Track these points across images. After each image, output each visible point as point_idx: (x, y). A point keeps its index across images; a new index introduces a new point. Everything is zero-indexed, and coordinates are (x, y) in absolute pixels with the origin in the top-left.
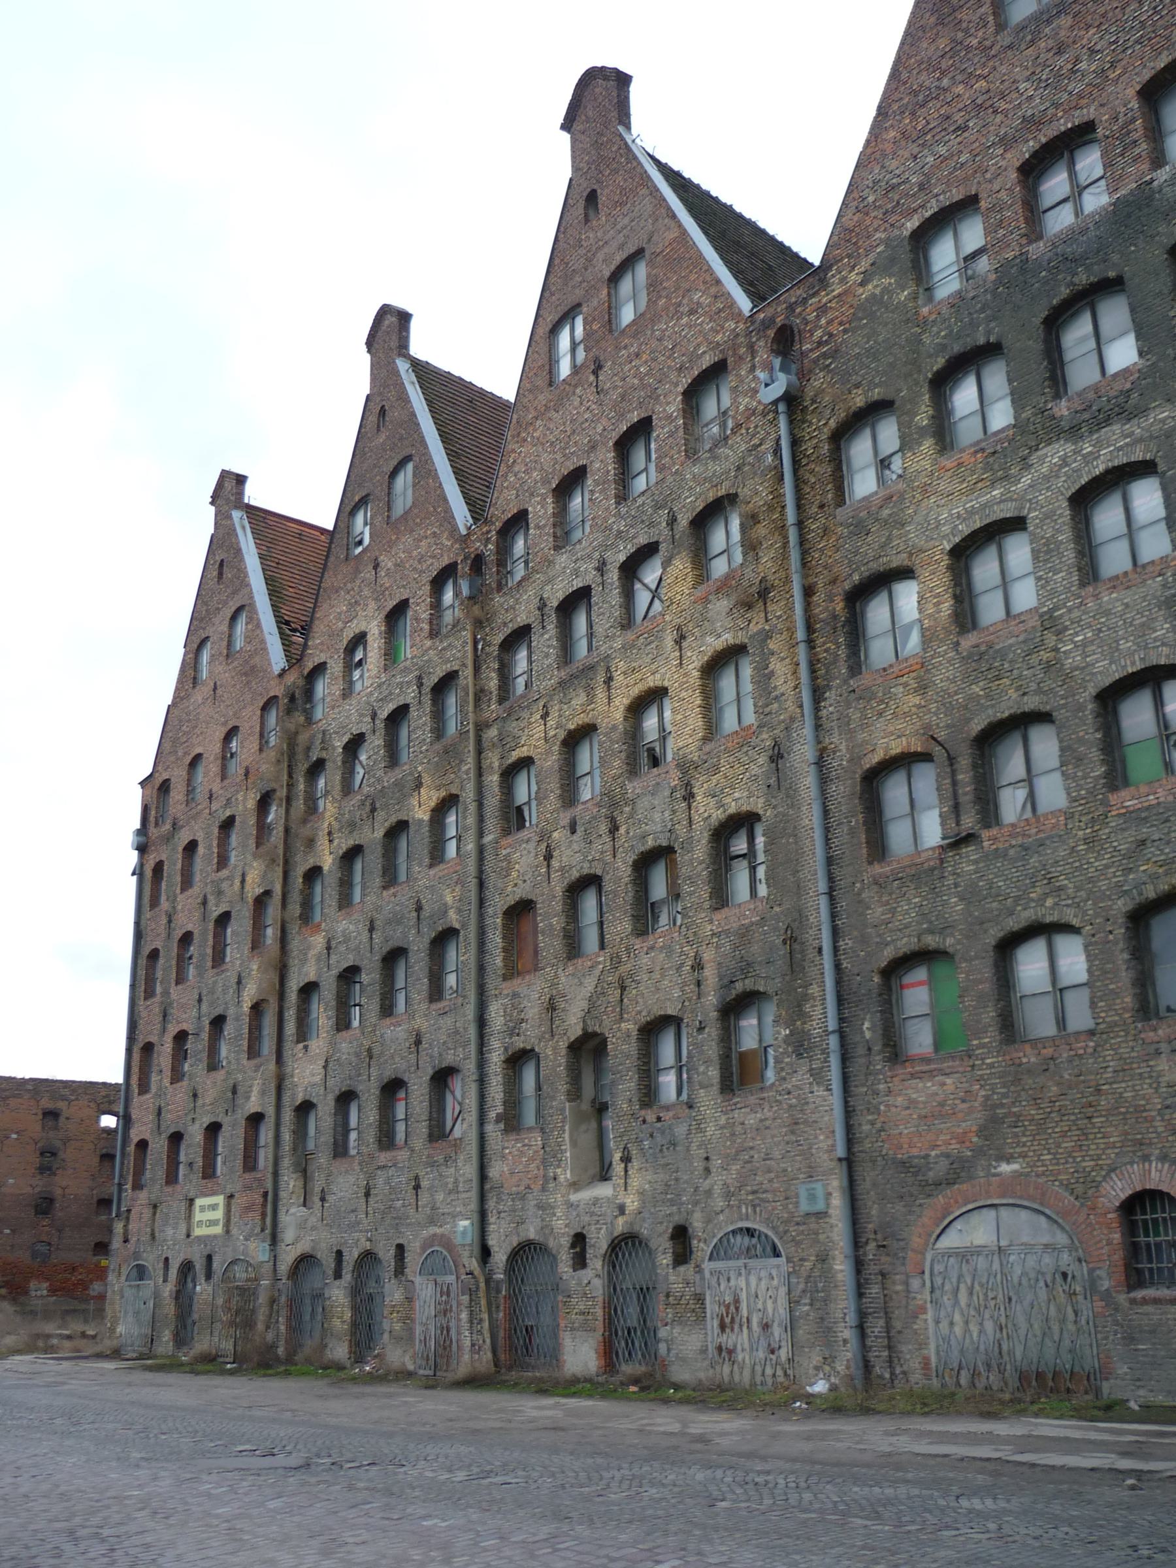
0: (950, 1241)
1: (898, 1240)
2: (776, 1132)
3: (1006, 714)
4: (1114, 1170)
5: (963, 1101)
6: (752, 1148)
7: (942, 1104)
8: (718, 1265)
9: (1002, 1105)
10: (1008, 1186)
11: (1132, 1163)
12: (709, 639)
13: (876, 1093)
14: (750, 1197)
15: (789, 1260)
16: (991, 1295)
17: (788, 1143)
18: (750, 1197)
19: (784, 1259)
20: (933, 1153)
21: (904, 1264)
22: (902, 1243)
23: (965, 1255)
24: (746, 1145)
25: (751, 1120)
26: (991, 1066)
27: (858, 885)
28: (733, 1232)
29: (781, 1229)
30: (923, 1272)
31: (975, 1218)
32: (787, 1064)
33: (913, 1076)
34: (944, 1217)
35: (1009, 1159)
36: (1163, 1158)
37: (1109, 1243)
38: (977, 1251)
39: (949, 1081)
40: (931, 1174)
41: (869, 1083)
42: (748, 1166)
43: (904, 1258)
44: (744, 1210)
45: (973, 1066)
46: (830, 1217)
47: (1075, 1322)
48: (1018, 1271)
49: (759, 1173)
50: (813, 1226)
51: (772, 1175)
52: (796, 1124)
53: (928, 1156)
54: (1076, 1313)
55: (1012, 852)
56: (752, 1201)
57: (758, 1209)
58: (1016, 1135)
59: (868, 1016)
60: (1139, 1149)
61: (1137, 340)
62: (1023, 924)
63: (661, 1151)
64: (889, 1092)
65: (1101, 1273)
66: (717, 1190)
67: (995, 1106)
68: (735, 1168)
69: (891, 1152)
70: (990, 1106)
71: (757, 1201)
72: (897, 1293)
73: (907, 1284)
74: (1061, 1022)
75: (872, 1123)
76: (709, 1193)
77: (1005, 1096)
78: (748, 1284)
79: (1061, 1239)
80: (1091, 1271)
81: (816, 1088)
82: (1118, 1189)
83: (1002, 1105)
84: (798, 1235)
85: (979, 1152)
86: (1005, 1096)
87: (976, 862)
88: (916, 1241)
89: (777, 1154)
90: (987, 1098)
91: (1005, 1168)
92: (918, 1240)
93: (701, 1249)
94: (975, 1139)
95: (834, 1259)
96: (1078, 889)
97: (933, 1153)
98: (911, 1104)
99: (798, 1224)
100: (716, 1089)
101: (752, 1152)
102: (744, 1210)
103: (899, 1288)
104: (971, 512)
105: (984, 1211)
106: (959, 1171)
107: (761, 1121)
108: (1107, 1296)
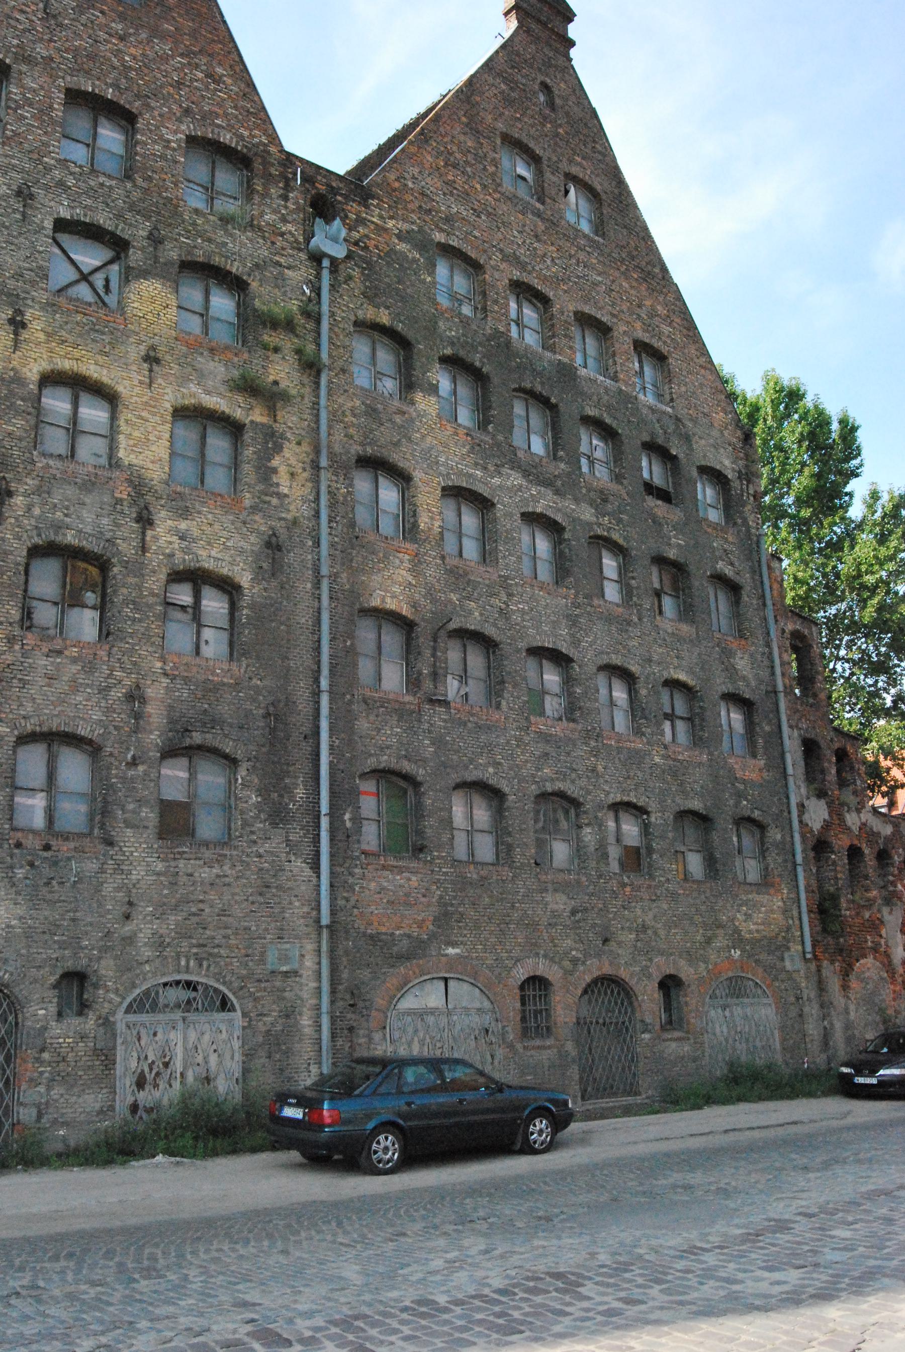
0: (408, 1003)
1: (364, 1000)
2: (237, 890)
3: (473, 627)
4: (518, 960)
5: (424, 896)
6: (201, 901)
7: (407, 895)
8: (131, 1018)
9: (452, 905)
10: (452, 963)
11: (529, 957)
12: (193, 388)
13: (352, 874)
14: (195, 950)
15: (245, 1015)
16: (438, 1045)
17: (253, 903)
18: (195, 950)
19: (239, 1013)
20: (397, 932)
21: (367, 1021)
22: (367, 1003)
23: (421, 1014)
24: (192, 897)
25: (206, 874)
26: (446, 874)
27: (348, 697)
28: (165, 985)
29: (236, 985)
30: (385, 1028)
31: (428, 986)
32: (259, 829)
33: (384, 868)
34: (406, 985)
35: (454, 944)
36: (545, 956)
37: (514, 1010)
38: (432, 1012)
39: (414, 878)
40: (395, 949)
41: (347, 865)
42: (195, 919)
43: (369, 1016)
44: (183, 963)
45: (432, 871)
46: (300, 976)
47: (492, 1063)
48: (458, 1027)
49: (211, 926)
50: (278, 984)
51: (229, 932)
52: (268, 887)
53: (392, 934)
54: (492, 1056)
55: (469, 725)
56: (196, 954)
57: (205, 964)
58: (460, 927)
59: (350, 809)
60: (532, 948)
61: (64, 232)
62: (474, 778)
63: (47, 884)
64: (363, 877)
65: (509, 1029)
66: (143, 937)
67: (445, 905)
68: (173, 919)
69: (362, 927)
70: (441, 902)
71: (204, 955)
72: (360, 1045)
73: (370, 1039)
74: (471, 852)
75: (347, 900)
76: (130, 940)
77: (455, 898)
78: (185, 1038)
79: (487, 1004)
80: (504, 1027)
81: (293, 858)
82: (521, 973)
83: (452, 905)
84: (258, 991)
85: (433, 936)
86: (455, 898)
87: (445, 721)
88: (380, 1002)
89: (237, 911)
90: (441, 897)
91: (451, 951)
92: (381, 1002)
93: (110, 997)
94: (431, 927)
95: (300, 1014)
96: (511, 769)
97: (397, 932)
98: (382, 890)
99: (259, 981)
100: (151, 833)
101: (201, 906)
102: (183, 963)
103: (362, 1040)
104: (460, 473)
105: (435, 981)
106: (417, 950)
107: (218, 876)
108: (511, 1046)
